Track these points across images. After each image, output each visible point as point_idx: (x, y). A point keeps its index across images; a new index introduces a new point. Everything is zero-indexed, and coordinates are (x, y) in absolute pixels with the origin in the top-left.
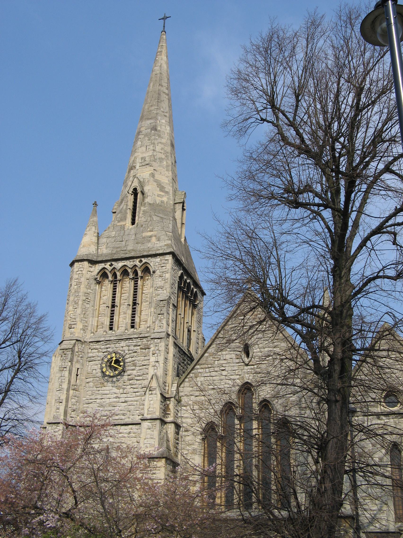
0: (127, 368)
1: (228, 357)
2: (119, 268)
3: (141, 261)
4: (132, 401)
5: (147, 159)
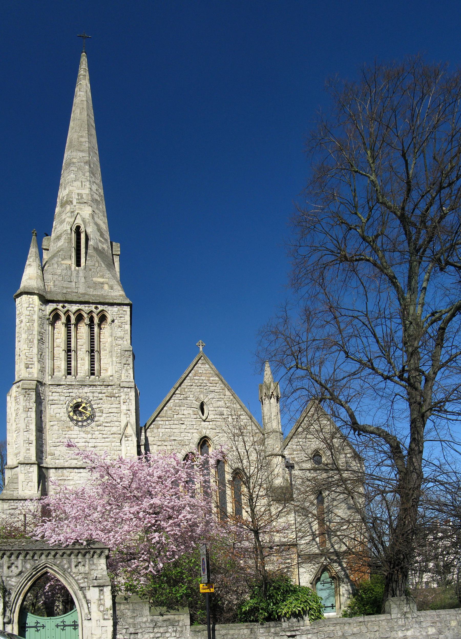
1: (185, 412)
2: (74, 311)
3: (96, 308)
4: (102, 446)
5: (84, 196)
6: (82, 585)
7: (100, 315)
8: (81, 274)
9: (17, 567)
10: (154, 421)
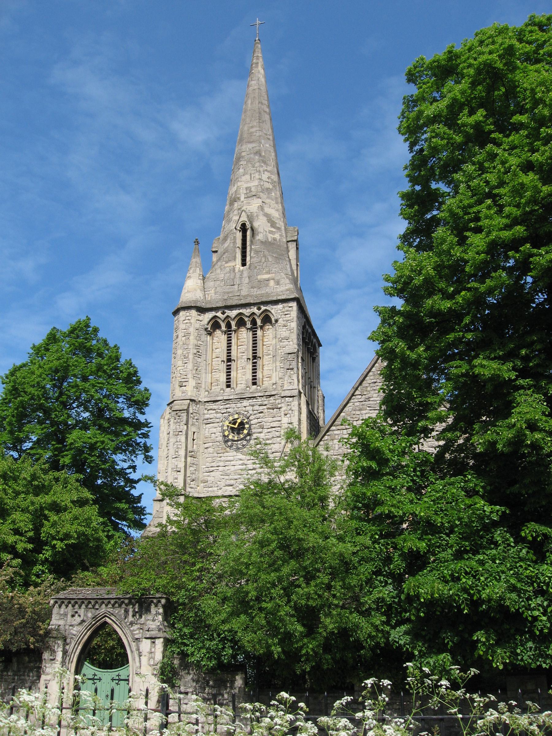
0: (253, 431)
2: (234, 316)
5: (253, 189)
6: (136, 636)
7: (262, 316)
8: (245, 274)
9: (80, 616)
10: (328, 431)
